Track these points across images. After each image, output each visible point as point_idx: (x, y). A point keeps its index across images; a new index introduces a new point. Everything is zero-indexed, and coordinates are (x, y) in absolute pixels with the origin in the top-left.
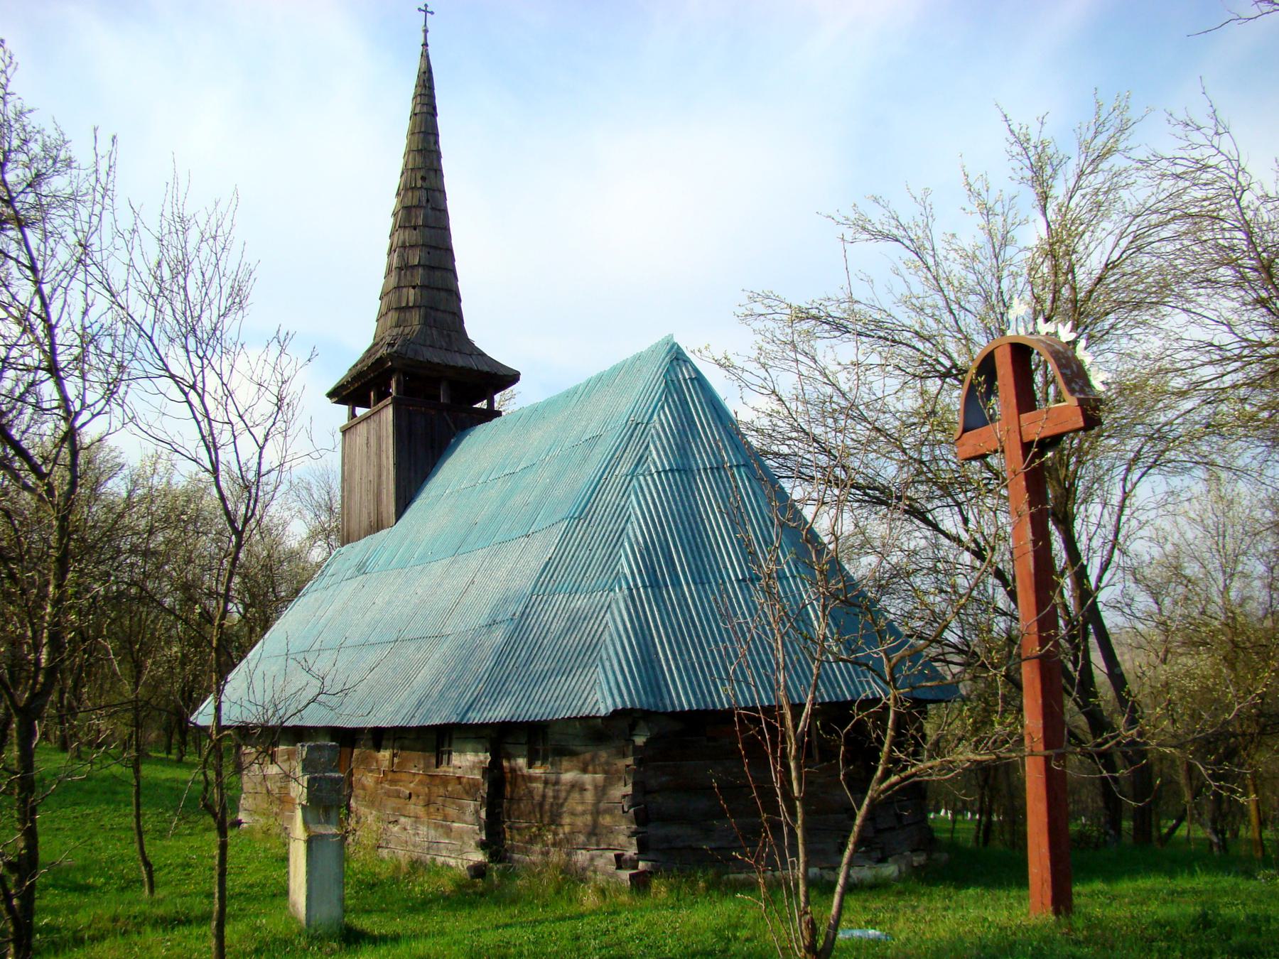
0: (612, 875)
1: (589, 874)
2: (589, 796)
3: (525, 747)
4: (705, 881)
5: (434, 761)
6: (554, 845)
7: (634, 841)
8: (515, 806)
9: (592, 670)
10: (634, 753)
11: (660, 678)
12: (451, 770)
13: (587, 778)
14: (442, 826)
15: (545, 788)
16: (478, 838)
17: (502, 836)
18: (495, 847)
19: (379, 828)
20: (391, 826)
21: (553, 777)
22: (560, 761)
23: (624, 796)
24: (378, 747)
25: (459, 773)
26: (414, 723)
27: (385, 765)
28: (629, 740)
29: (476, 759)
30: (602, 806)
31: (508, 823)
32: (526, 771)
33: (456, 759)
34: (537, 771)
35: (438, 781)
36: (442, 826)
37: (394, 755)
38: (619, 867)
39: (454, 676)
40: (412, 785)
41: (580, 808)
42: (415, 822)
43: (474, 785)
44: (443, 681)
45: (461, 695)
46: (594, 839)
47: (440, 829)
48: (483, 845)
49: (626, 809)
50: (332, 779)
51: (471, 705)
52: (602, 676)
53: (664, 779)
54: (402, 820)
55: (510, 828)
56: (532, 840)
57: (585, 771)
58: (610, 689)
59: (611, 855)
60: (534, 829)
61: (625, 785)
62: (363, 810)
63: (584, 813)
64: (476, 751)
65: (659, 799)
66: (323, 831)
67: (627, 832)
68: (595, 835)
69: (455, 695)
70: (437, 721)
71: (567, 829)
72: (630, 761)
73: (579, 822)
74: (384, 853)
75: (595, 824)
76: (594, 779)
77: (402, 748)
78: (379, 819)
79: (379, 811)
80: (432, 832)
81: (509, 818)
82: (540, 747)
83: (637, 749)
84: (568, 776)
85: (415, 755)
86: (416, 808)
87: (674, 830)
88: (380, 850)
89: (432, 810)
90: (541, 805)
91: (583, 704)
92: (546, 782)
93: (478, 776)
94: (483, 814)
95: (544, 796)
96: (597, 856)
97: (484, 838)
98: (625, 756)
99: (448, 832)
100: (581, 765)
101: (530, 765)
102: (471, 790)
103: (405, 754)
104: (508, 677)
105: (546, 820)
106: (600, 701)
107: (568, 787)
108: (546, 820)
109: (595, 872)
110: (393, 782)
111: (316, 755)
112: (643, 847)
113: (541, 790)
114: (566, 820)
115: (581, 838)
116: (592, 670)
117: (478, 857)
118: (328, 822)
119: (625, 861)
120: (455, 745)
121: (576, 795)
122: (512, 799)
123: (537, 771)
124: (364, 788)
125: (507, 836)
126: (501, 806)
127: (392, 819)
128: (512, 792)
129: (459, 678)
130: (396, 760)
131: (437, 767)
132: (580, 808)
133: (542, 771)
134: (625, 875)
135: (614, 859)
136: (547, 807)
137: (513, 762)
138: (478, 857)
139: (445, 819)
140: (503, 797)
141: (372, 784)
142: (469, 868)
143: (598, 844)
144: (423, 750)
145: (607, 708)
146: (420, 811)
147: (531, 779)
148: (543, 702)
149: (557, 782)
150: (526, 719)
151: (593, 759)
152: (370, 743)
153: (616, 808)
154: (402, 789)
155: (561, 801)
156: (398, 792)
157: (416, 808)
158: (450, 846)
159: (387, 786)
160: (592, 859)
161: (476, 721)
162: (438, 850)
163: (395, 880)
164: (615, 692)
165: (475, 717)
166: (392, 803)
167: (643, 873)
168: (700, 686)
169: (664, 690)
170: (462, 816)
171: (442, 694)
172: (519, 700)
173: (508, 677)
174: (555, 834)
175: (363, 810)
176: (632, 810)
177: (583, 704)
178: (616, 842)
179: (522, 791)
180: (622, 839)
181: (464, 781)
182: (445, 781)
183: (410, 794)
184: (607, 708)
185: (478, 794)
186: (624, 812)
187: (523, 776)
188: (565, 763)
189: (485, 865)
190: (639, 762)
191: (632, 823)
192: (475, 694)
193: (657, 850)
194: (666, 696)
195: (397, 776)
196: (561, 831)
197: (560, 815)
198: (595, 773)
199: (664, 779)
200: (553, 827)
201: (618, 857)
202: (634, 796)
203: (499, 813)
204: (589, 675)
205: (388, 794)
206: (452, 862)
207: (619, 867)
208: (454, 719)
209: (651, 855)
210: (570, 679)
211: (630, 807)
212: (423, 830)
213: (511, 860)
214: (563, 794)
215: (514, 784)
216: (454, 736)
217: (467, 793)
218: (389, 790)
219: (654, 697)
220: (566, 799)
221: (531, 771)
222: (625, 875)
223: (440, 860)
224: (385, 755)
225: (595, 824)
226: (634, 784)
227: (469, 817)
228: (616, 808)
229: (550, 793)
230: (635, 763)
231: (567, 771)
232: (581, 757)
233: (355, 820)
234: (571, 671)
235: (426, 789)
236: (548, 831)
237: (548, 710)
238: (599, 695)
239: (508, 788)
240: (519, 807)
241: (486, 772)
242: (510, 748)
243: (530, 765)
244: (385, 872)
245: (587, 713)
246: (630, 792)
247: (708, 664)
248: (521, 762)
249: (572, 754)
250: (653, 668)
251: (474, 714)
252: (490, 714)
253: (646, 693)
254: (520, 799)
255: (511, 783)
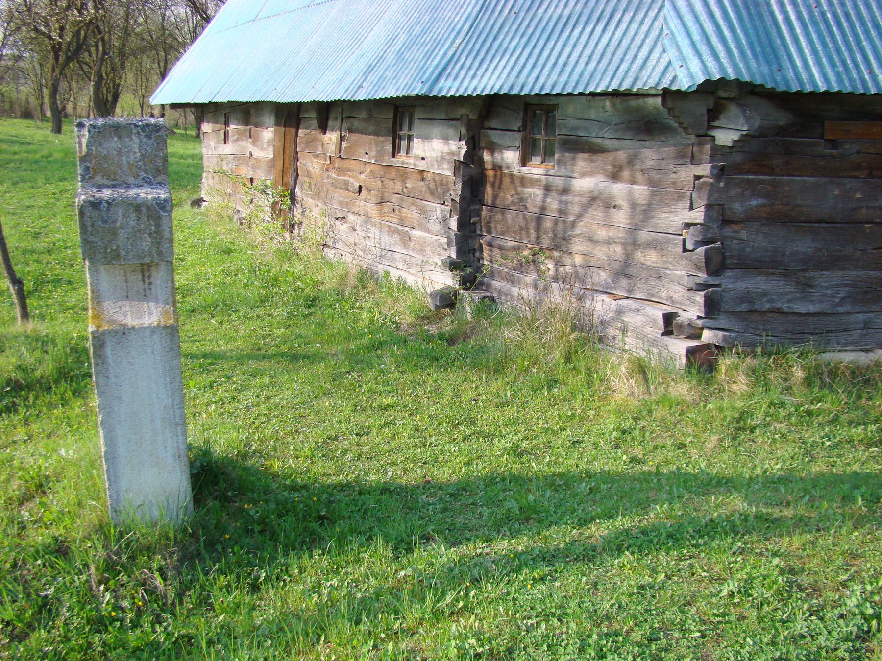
0: (653, 343)
1: (612, 332)
2: (621, 217)
3: (519, 136)
4: (803, 368)
5: (389, 147)
6: (556, 279)
7: (700, 297)
8: (499, 217)
9: (652, 14)
10: (713, 157)
11: (774, 33)
12: (411, 161)
13: (618, 189)
14: (397, 231)
15: (545, 196)
16: (445, 255)
17: (477, 254)
18: (469, 270)
19: (324, 225)
20: (338, 223)
21: (559, 182)
22: (574, 159)
23: (688, 225)
24: (323, 127)
25: (422, 165)
26: (361, 96)
27: (332, 149)
28: (704, 136)
29: (446, 149)
30: (644, 235)
31: (487, 238)
32: (516, 169)
33: (418, 147)
34: (535, 171)
35: (393, 173)
36: (397, 231)
37: (342, 139)
38: (668, 333)
39: (418, 30)
40: (362, 176)
41: (602, 234)
42: (366, 222)
43: (442, 184)
44: (402, 38)
45: (428, 56)
46: (624, 282)
47: (396, 236)
48: (453, 266)
49: (689, 246)
50: (138, 207)
51: (444, 69)
52: (674, 23)
53: (754, 203)
54: (351, 217)
55: (490, 245)
56: (522, 267)
57: (615, 177)
58: (693, 44)
59: (657, 313)
60: (526, 253)
61: (691, 208)
62: (309, 201)
63: (608, 242)
64: (446, 138)
65: (744, 234)
66: (130, 321)
67: (688, 282)
68: (628, 276)
69: (420, 56)
70: (391, 92)
71: (578, 260)
72: (704, 169)
73: (601, 253)
74: (330, 253)
75: (628, 260)
76: (630, 193)
77: (351, 131)
78: (324, 214)
79: (325, 203)
80: (386, 238)
81: (489, 232)
82: (541, 137)
83: (718, 152)
84: (584, 184)
85: (366, 138)
86: (367, 204)
87: (759, 283)
88: (326, 249)
89: (386, 210)
90: (539, 220)
91: (643, 66)
92: (548, 189)
93: (447, 171)
94: (454, 224)
95: (543, 208)
96: (631, 310)
97: (454, 255)
98: (694, 160)
99: (406, 239)
100: (609, 168)
101: (524, 163)
102: (438, 189)
103: (355, 137)
104: (501, 28)
105: (546, 242)
106: (676, 64)
107: (584, 200)
108: (546, 242)
109: (624, 331)
110: (341, 171)
111: (113, 144)
112: (712, 307)
113: (539, 199)
114: (578, 246)
115: (602, 276)
116: (652, 14)
117: (446, 280)
118: (145, 296)
119: (681, 326)
120: (418, 127)
121: (596, 214)
122: (494, 206)
123: (536, 170)
124: (309, 175)
125: (485, 255)
126: (479, 215)
127: (339, 215)
128: (495, 197)
129: (424, 32)
130: (344, 145)
131: (393, 156)
132: (602, 234)
133: (541, 171)
134: (679, 347)
135: (661, 321)
136: (548, 224)
137: (498, 157)
138: (446, 280)
139: (402, 222)
140: (482, 203)
141: (318, 172)
142: (434, 295)
143: (630, 291)
144: (376, 134)
145: (691, 76)
146: (371, 209)
147: (524, 181)
148: (565, 65)
149: (565, 191)
150: (536, 91)
151: (631, 162)
152: (315, 123)
153: (668, 242)
154: (351, 180)
155: (571, 218)
156: (346, 183)
157: (367, 204)
158: (407, 258)
159: (334, 175)
160: (620, 312)
161: (451, 93)
162: (393, 260)
163: (340, 294)
164: (703, 49)
165: (449, 88)
166: (339, 195)
167: (707, 346)
168: (838, 51)
169: (782, 52)
170: (424, 222)
171: (400, 56)
172: (522, 60)
173: (501, 28)
174: (558, 263)
175: (309, 201)
176: (701, 250)
177: (643, 66)
178: (664, 294)
179: (507, 197)
180: (678, 292)
181: (429, 176)
182: (403, 174)
183: (360, 187)
184: (691, 76)
185: (447, 197)
186: (685, 250)
187: (512, 176)
188: (582, 162)
189: (456, 294)
190: (721, 173)
191: (698, 268)
192: (450, 53)
193: (733, 313)
194: (786, 64)
195: (345, 164)
196: (567, 260)
197: (566, 239)
198: (633, 182)
199: (754, 203)
200: (556, 254)
201: (669, 318)
202: (704, 228)
203: (474, 224)
204: (648, 22)
205: (335, 185)
206: (410, 280)
207: (668, 333)
208: (417, 90)
209: (723, 322)
210: (611, 28)
211: (698, 244)
212: (374, 232)
213: (488, 287)
214: (575, 209)
215: (498, 185)
216: (416, 117)
217: (432, 194)
218: (336, 180)
219: (768, 63)
220: (579, 217)
221: (525, 170)
222: (679, 347)
223: (394, 274)
224: (331, 137)
225: (628, 260)
226: (709, 207)
227: (435, 226)
228: (668, 242)
229: (553, 204)
230: (713, 175)
231: (584, 175)
232: (610, 157)
233: (300, 210)
234: (612, 16)
235: (379, 183)
236: (550, 257)
237: (575, 77)
238: (672, 54)
239: (489, 191)
240: (504, 219)
241: (459, 166)
242: (495, 136)
243: (524, 163)
244: (329, 280)
245: (652, 83)
246: (700, 220)
247: (847, 16)
248: (511, 157)
249: (594, 150)
250: (760, 16)
251: (449, 83)
252: (475, 82)
253: (755, 55)
254: (505, 209)
255: (493, 185)
